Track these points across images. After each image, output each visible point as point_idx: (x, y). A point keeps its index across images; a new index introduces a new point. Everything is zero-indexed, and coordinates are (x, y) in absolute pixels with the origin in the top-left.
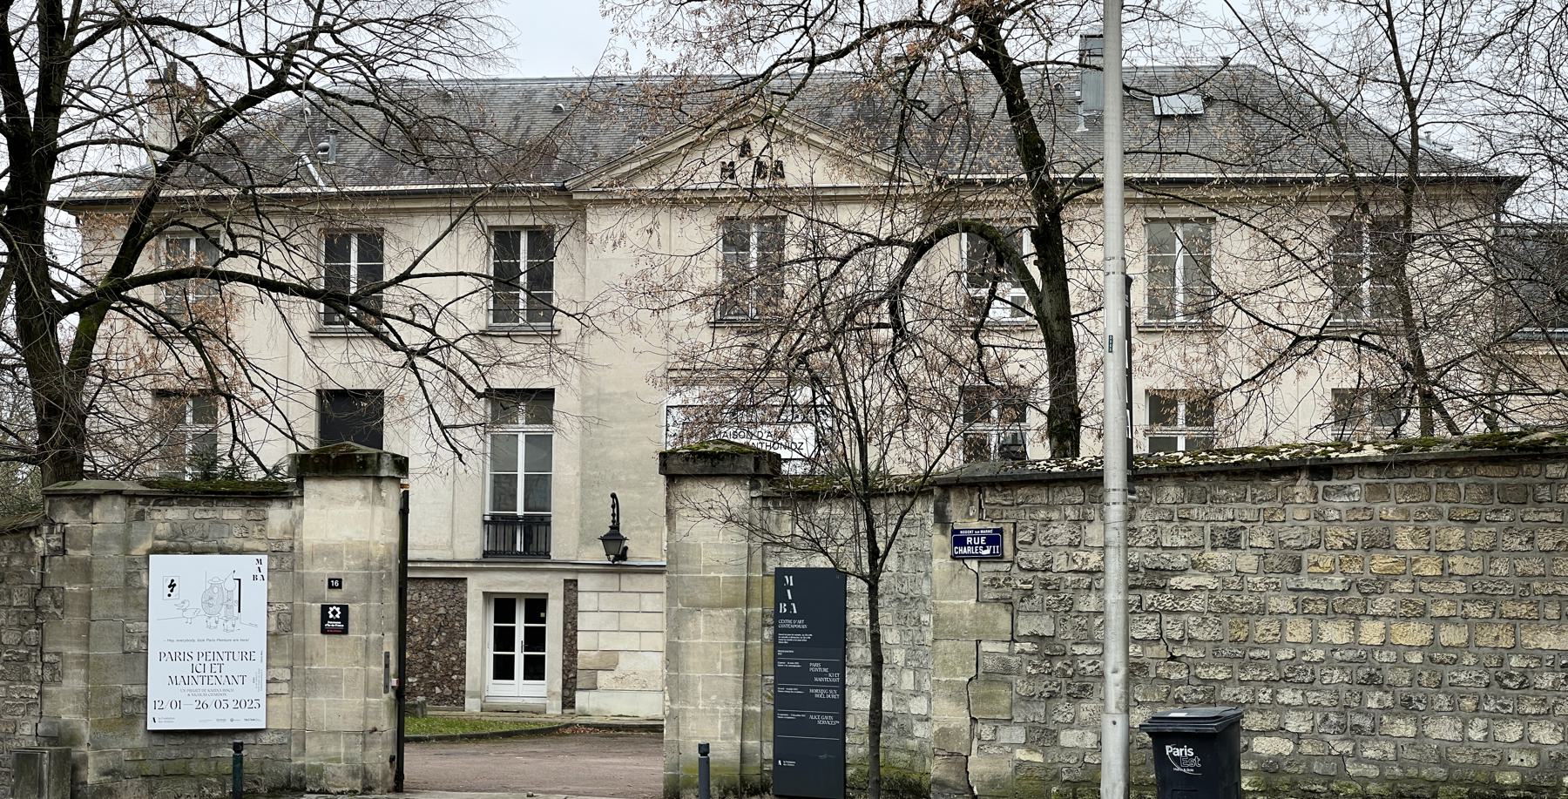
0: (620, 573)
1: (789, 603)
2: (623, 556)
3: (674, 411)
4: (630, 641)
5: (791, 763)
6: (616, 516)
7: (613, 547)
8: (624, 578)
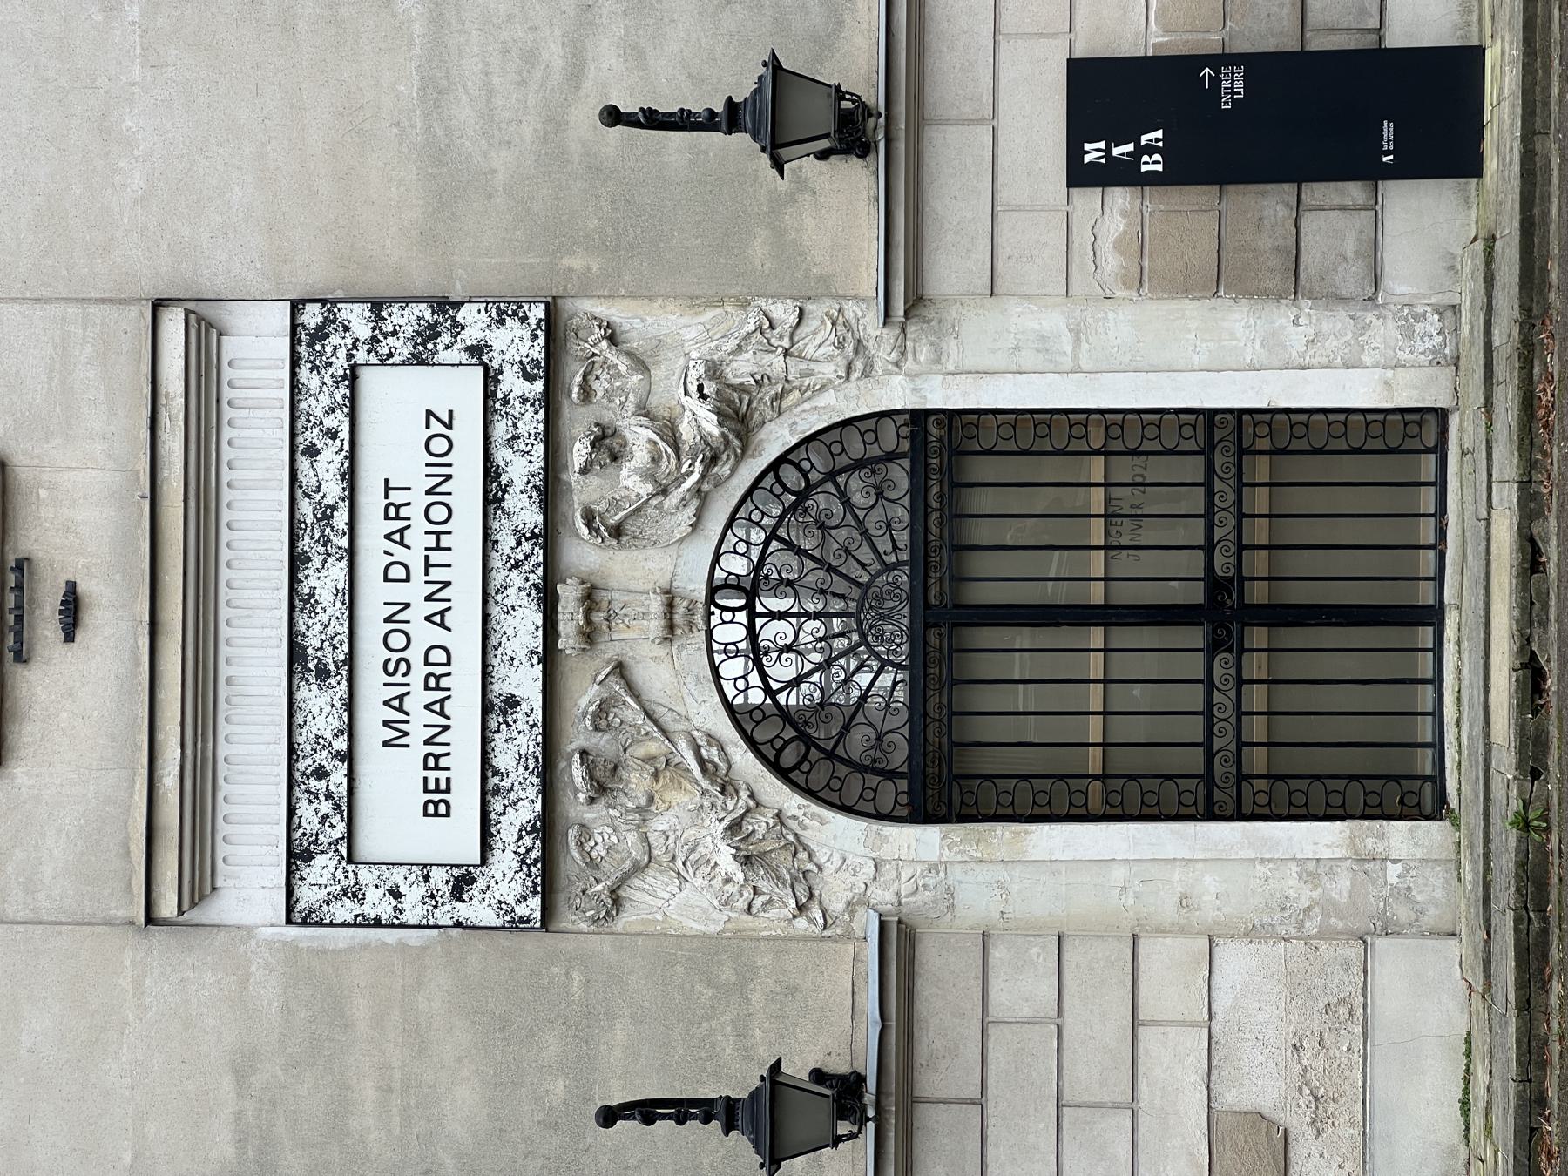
0: (910, 1101)
1: (1140, 151)
2: (844, 1093)
3: (308, 896)
4: (1174, 1064)
5: (1388, 130)
6: (683, 1110)
7: (810, 1114)
8: (930, 1083)
